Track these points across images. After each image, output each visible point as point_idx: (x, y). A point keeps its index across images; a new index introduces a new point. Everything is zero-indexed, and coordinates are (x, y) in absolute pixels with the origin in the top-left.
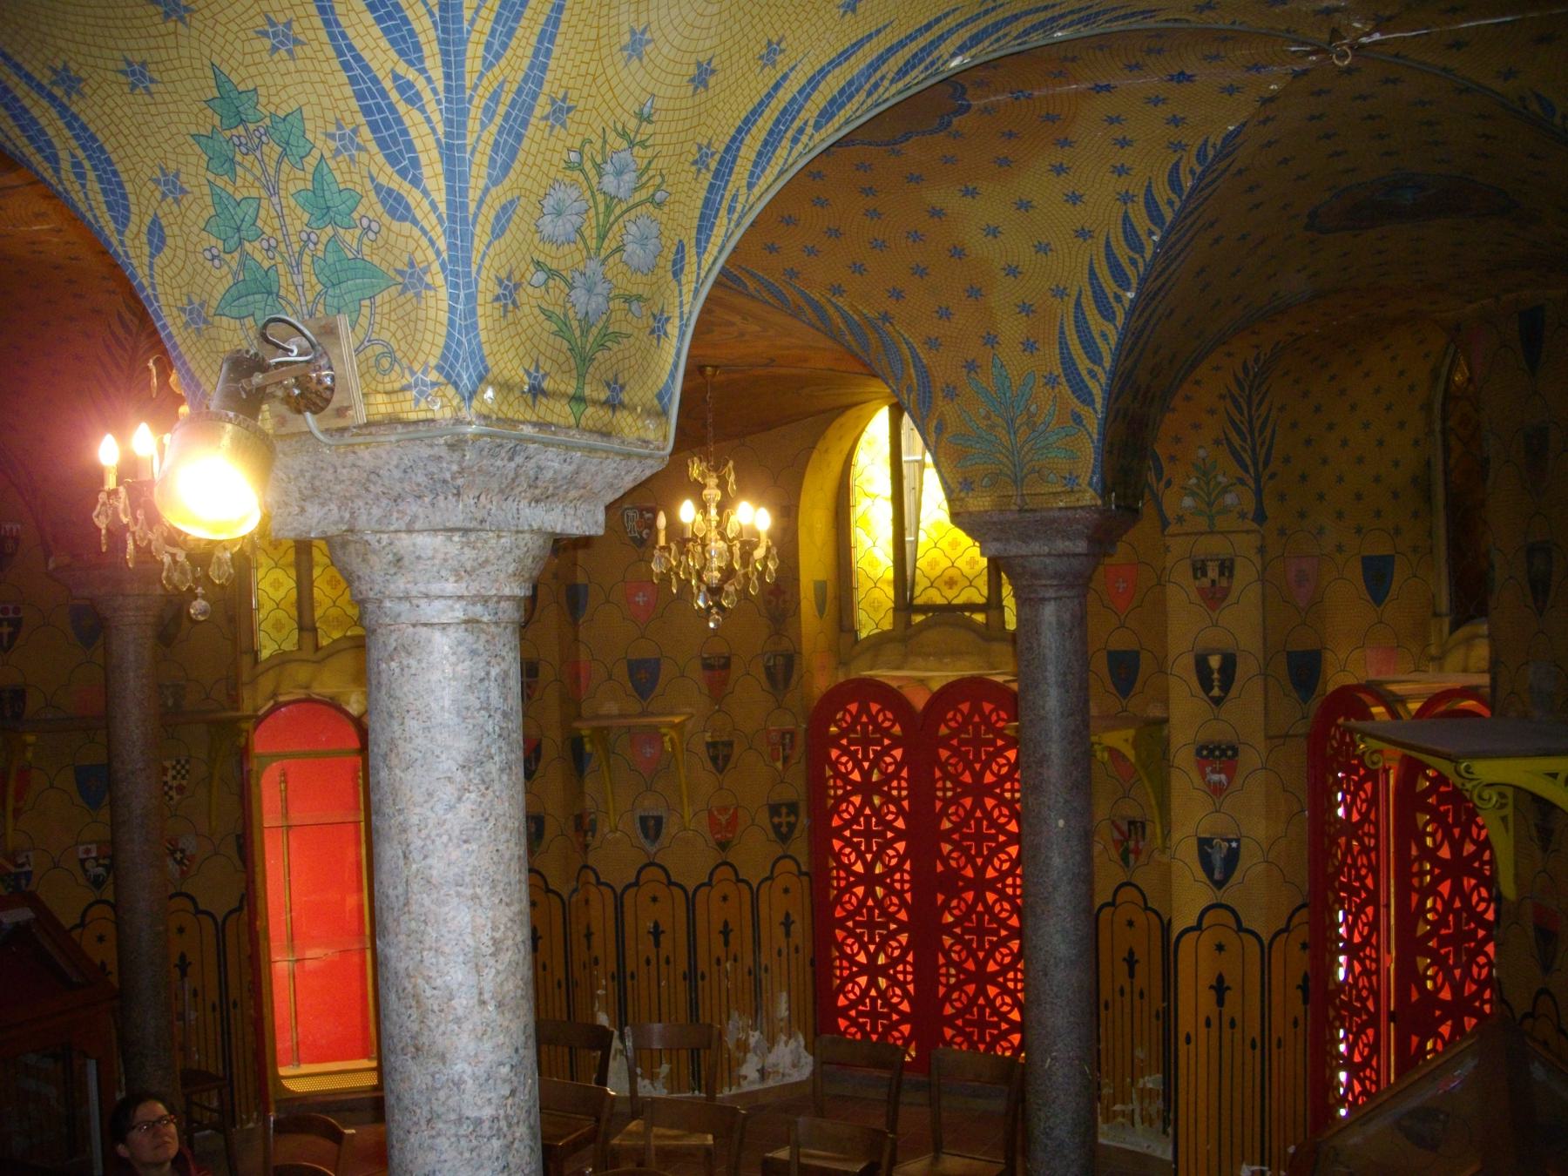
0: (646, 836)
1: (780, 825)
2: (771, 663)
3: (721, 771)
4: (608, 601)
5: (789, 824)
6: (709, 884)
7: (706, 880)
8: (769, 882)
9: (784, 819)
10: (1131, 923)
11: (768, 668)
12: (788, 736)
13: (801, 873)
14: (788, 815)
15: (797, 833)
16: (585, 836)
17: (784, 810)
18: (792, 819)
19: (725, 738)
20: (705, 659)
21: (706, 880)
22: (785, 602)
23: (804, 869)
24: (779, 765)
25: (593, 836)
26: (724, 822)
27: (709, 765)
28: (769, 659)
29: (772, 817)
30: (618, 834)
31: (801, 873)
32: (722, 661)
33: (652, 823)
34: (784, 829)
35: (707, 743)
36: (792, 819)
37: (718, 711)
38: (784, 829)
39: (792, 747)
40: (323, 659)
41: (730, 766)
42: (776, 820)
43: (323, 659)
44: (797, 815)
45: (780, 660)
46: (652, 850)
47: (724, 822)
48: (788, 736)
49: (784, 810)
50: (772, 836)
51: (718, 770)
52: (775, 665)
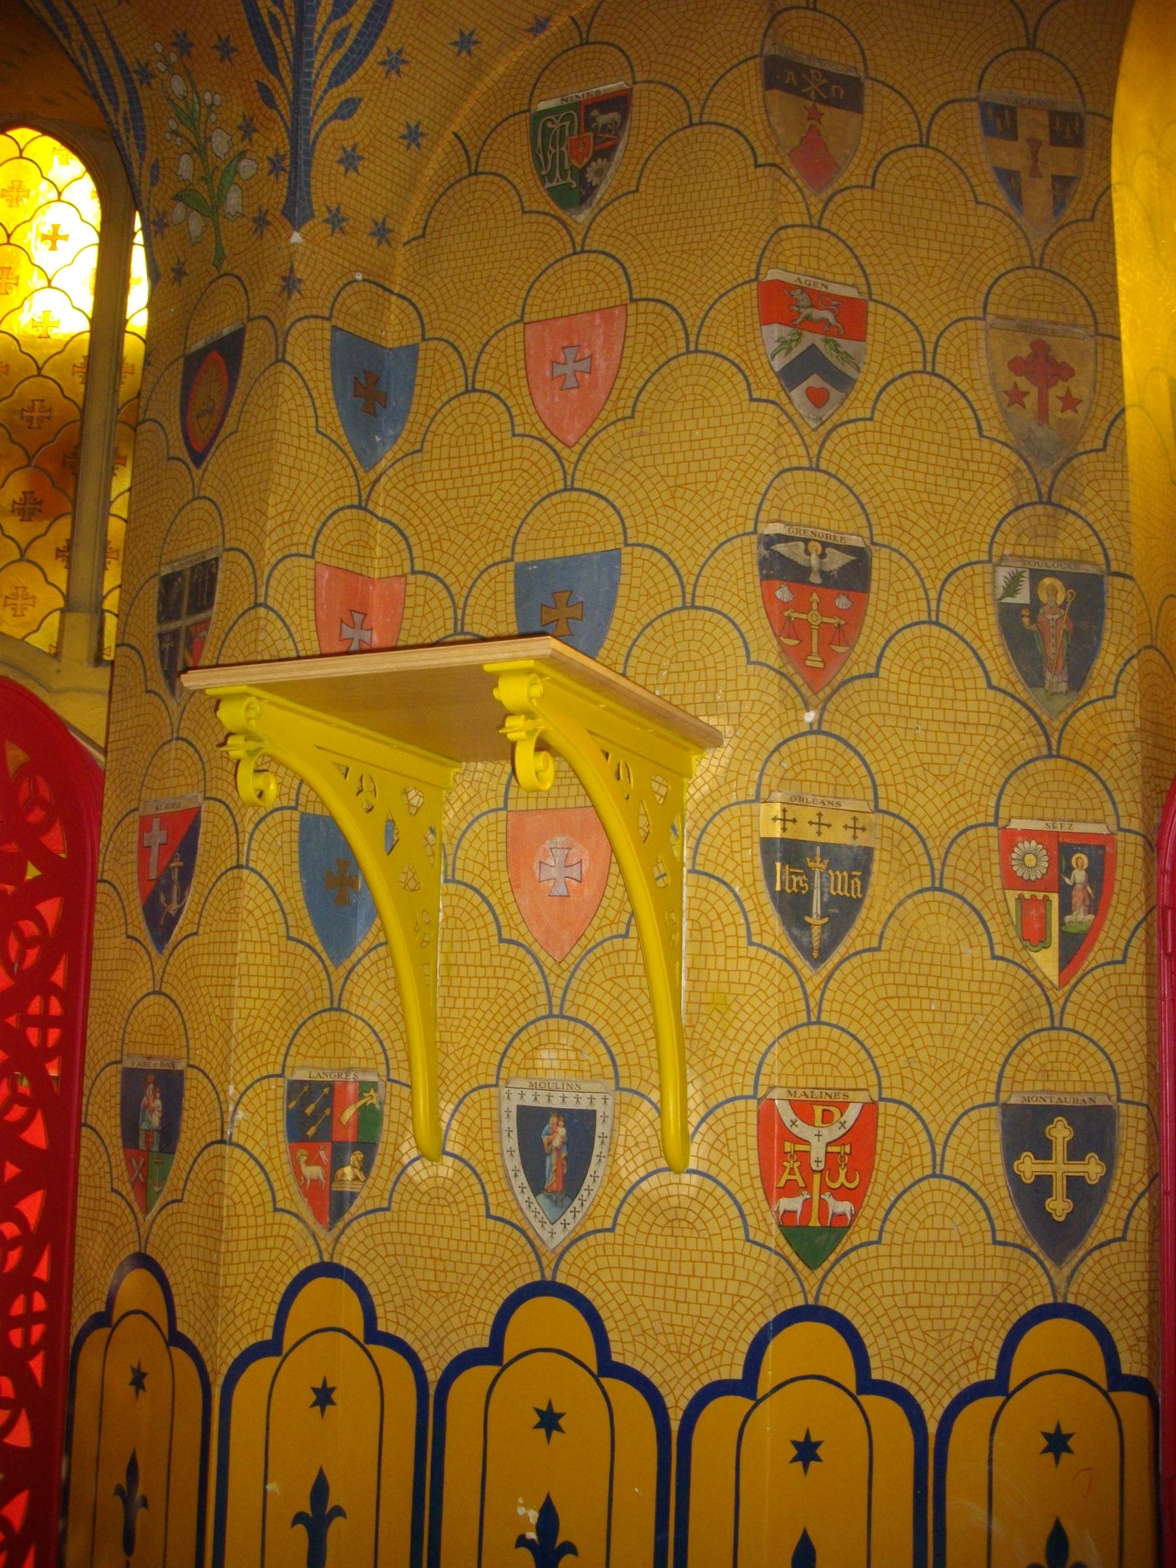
0: (537, 1183)
1: (1043, 1184)
2: (1023, 597)
3: (816, 957)
4: (470, 389)
5: (1075, 1185)
6: (747, 1386)
7: (737, 1374)
8: (991, 1403)
9: (1059, 1167)
10: (549, 1421)
11: (1009, 618)
12: (1081, 860)
13: (1117, 1380)
14: (1075, 1152)
15: (1106, 1223)
16: (337, 1162)
17: (1060, 1132)
18: (1092, 1169)
19: (838, 836)
20: (769, 541)
21: (737, 1374)
22: (1069, 402)
23: (1130, 1364)
24: (1047, 961)
25: (366, 1167)
26: (817, 1151)
27: (773, 927)
28: (1012, 587)
29: (1011, 1154)
30: (446, 1168)
31: (1117, 1380)
32: (836, 561)
33: (557, 1135)
34: (1059, 1206)
35: (767, 844)
36: (1092, 1169)
37: (816, 730)
38: (1059, 1206)
39: (1098, 905)
40: (574, 1242)
41: (852, 941)
42: (1028, 1167)
43: (574, 1242)
44: (1108, 1157)
45: (1054, 592)
46: (554, 1236)
47: (817, 1151)
48: (1081, 860)
49: (1060, 1132)
50: (1012, 1224)
51: (806, 951)
52: (1035, 605)
